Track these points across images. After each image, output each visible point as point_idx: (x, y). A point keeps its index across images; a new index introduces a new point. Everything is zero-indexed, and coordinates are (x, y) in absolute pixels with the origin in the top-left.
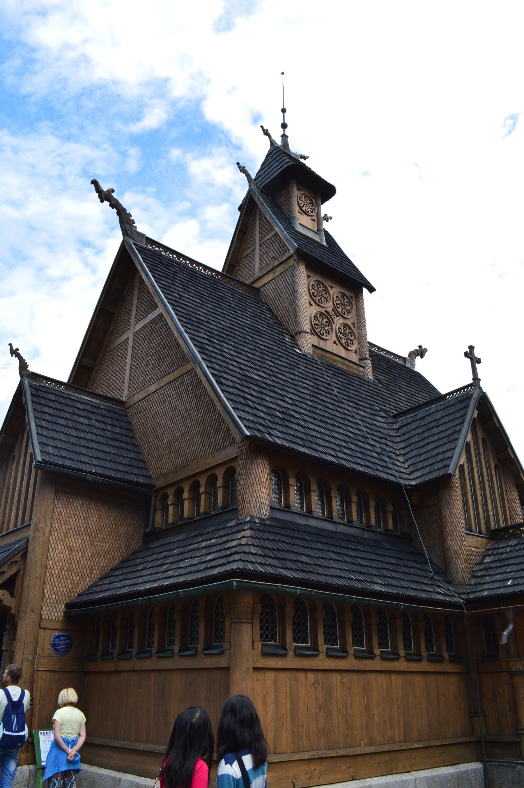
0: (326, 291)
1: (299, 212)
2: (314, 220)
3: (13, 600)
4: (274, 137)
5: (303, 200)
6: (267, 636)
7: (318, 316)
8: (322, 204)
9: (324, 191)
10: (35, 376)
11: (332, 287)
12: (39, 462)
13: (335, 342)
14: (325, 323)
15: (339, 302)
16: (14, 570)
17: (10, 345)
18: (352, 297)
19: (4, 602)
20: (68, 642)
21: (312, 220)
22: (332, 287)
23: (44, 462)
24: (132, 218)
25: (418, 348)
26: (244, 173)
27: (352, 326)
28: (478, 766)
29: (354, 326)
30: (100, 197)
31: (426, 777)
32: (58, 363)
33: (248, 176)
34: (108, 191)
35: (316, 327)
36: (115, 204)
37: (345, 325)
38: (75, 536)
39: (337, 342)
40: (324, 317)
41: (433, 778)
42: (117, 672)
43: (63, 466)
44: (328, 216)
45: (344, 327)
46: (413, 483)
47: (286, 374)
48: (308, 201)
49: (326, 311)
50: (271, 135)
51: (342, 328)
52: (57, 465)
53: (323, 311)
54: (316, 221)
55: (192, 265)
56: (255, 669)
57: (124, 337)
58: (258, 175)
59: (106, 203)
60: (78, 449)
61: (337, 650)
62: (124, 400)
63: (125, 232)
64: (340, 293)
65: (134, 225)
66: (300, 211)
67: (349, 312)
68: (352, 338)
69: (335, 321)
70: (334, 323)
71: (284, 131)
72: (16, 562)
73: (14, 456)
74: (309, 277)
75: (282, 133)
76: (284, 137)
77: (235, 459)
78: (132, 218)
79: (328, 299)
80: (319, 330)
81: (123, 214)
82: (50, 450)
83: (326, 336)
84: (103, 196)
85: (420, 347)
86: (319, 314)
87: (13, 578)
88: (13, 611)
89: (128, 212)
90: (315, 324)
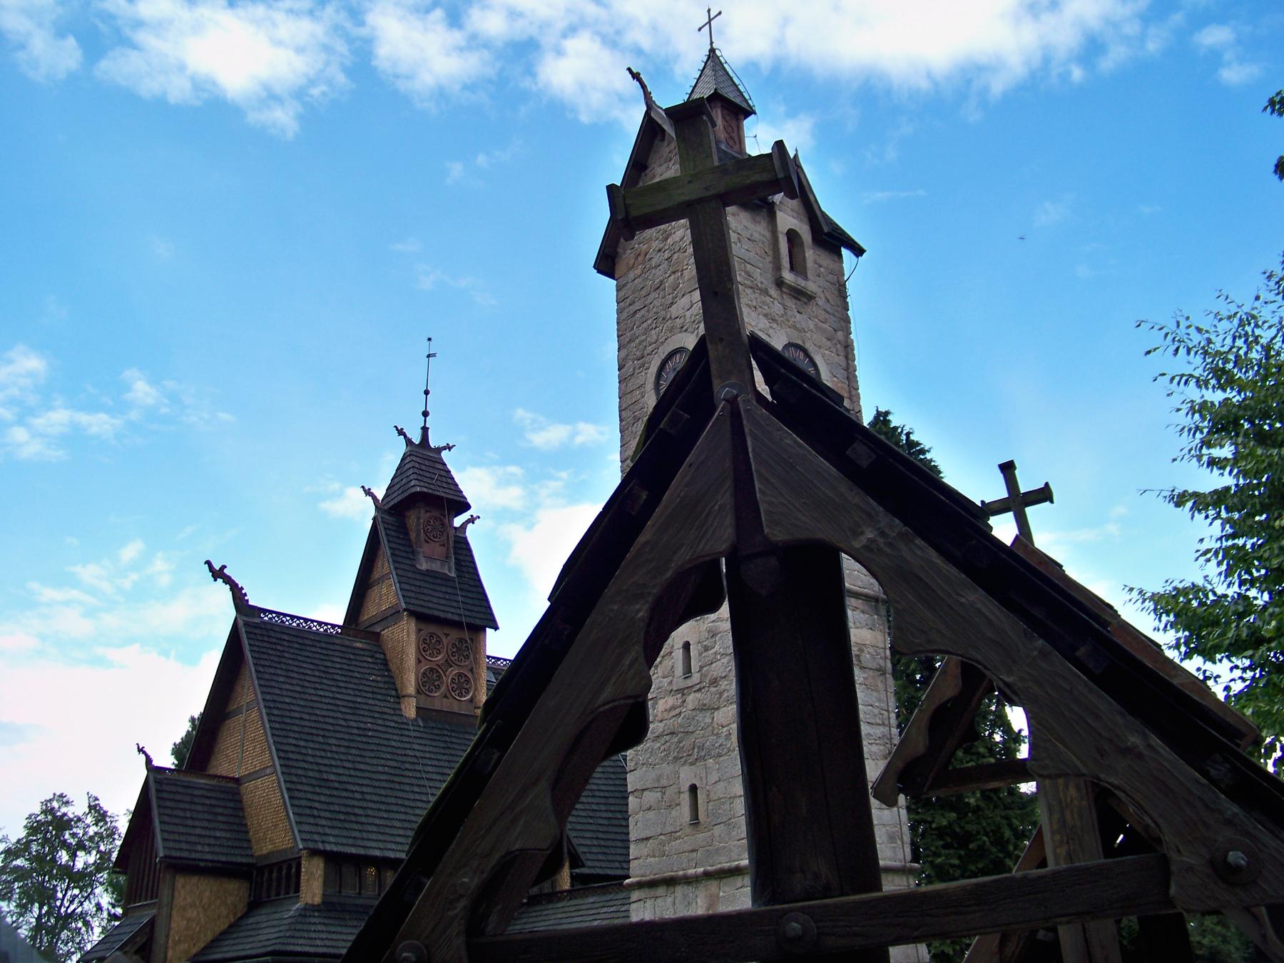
11: (447, 635)
13: (446, 696)
17: (208, 563)
22: (447, 635)
23: (165, 857)
27: (469, 675)
33: (374, 498)
36: (228, 580)
43: (181, 858)
52: (176, 858)
74: (420, 630)
76: (425, 430)
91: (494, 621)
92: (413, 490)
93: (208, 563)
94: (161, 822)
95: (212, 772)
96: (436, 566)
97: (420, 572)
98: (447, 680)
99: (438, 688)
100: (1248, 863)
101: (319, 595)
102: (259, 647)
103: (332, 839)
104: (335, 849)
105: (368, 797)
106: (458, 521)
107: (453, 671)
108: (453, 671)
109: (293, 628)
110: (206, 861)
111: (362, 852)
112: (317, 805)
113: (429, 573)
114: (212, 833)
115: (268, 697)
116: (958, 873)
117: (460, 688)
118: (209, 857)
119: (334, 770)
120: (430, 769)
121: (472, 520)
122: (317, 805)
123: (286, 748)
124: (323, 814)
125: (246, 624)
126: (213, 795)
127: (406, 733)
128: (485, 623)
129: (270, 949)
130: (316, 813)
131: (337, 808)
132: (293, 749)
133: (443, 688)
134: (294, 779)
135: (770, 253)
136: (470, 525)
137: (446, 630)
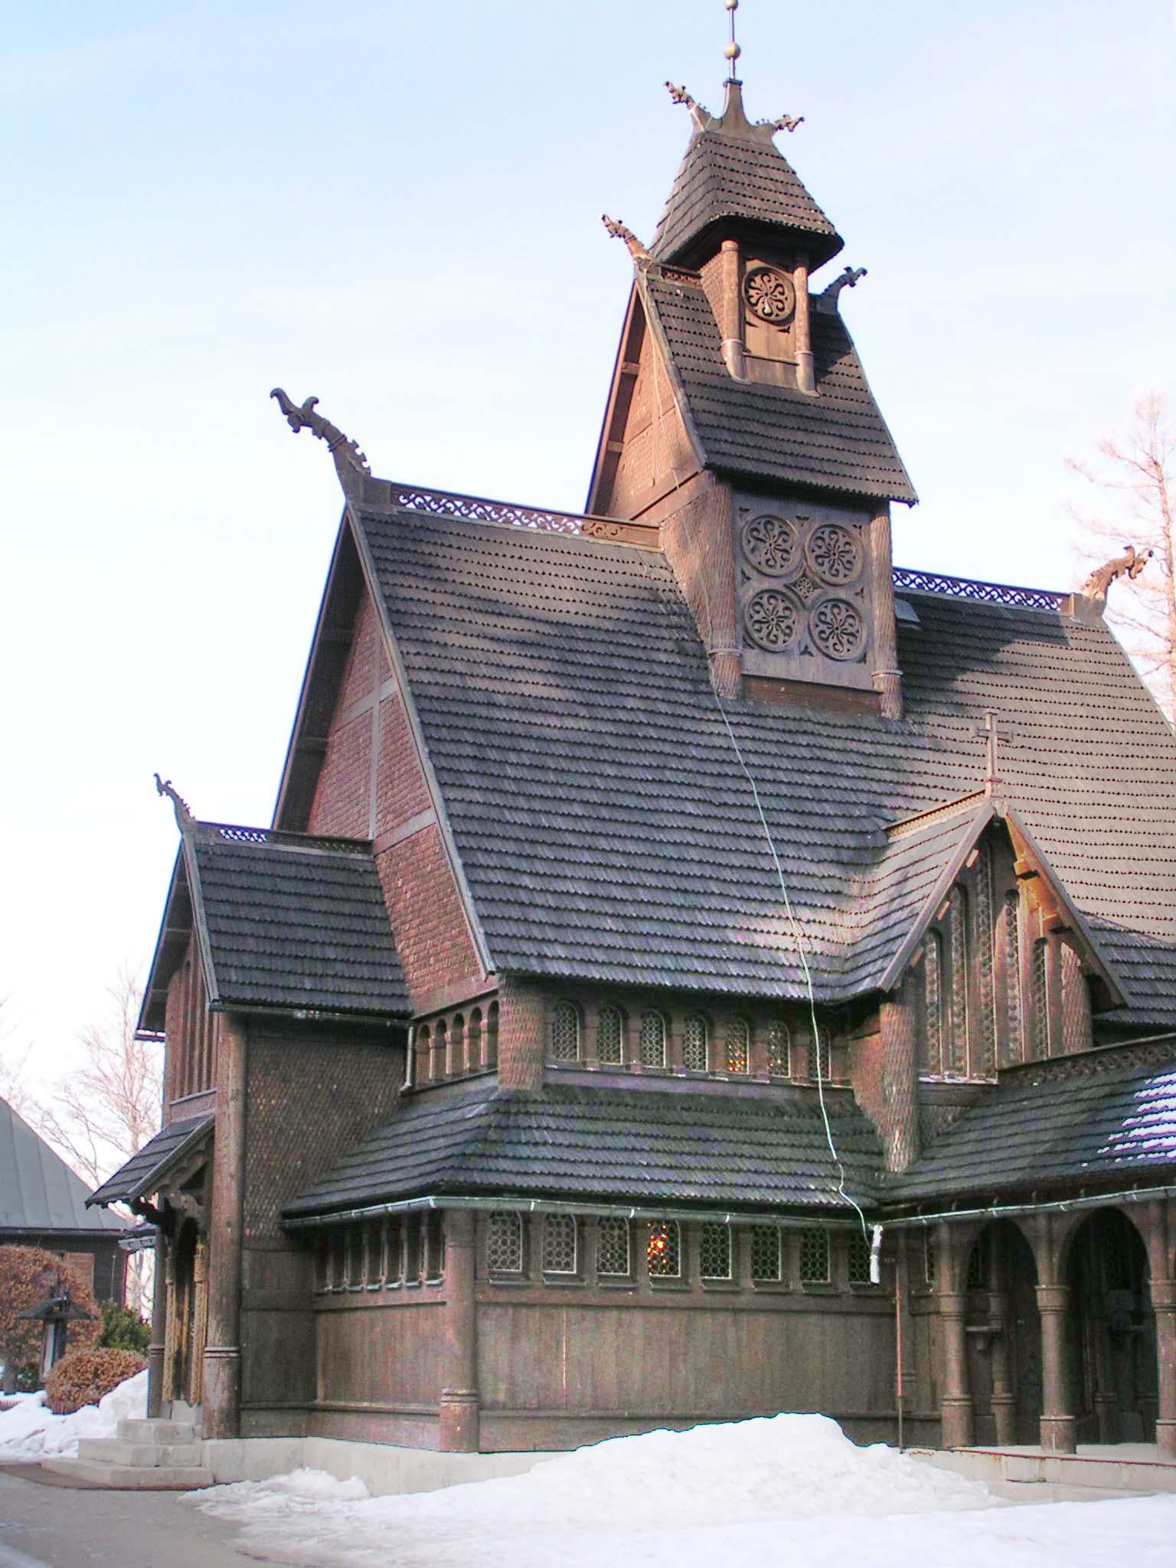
7: (764, 601)
8: (346, 508)
10: (205, 827)
13: (806, 651)
16: (199, 1163)
17: (278, 394)
20: (413, 1315)
24: (358, 452)
27: (856, 602)
30: (290, 422)
32: (246, 795)
35: (757, 626)
36: (324, 430)
38: (850, 841)
39: (812, 649)
42: (344, 1411)
44: (854, 270)
53: (776, 584)
57: (361, 708)
58: (117, 1180)
59: (306, 431)
60: (279, 964)
61: (573, 1276)
62: (370, 838)
65: (365, 465)
72: (199, 1152)
73: (188, 963)
75: (728, 75)
76: (734, 84)
77: (495, 992)
78: (358, 452)
80: (765, 632)
85: (848, 269)
86: (766, 596)
87: (202, 1170)
89: (350, 440)
91: (906, 484)
93: (278, 394)
94: (211, 931)
101: (520, 412)
102: (395, 553)
103: (560, 951)
105: (639, 863)
106: (820, 280)
109: (473, 525)
112: (527, 881)
114: (318, 952)
116: (719, 1247)
119: (565, 809)
121: (849, 278)
122: (527, 881)
124: (539, 899)
125: (364, 519)
129: (430, 1180)
130: (524, 896)
135: (771, 507)
136: (846, 290)
137: (802, 510)
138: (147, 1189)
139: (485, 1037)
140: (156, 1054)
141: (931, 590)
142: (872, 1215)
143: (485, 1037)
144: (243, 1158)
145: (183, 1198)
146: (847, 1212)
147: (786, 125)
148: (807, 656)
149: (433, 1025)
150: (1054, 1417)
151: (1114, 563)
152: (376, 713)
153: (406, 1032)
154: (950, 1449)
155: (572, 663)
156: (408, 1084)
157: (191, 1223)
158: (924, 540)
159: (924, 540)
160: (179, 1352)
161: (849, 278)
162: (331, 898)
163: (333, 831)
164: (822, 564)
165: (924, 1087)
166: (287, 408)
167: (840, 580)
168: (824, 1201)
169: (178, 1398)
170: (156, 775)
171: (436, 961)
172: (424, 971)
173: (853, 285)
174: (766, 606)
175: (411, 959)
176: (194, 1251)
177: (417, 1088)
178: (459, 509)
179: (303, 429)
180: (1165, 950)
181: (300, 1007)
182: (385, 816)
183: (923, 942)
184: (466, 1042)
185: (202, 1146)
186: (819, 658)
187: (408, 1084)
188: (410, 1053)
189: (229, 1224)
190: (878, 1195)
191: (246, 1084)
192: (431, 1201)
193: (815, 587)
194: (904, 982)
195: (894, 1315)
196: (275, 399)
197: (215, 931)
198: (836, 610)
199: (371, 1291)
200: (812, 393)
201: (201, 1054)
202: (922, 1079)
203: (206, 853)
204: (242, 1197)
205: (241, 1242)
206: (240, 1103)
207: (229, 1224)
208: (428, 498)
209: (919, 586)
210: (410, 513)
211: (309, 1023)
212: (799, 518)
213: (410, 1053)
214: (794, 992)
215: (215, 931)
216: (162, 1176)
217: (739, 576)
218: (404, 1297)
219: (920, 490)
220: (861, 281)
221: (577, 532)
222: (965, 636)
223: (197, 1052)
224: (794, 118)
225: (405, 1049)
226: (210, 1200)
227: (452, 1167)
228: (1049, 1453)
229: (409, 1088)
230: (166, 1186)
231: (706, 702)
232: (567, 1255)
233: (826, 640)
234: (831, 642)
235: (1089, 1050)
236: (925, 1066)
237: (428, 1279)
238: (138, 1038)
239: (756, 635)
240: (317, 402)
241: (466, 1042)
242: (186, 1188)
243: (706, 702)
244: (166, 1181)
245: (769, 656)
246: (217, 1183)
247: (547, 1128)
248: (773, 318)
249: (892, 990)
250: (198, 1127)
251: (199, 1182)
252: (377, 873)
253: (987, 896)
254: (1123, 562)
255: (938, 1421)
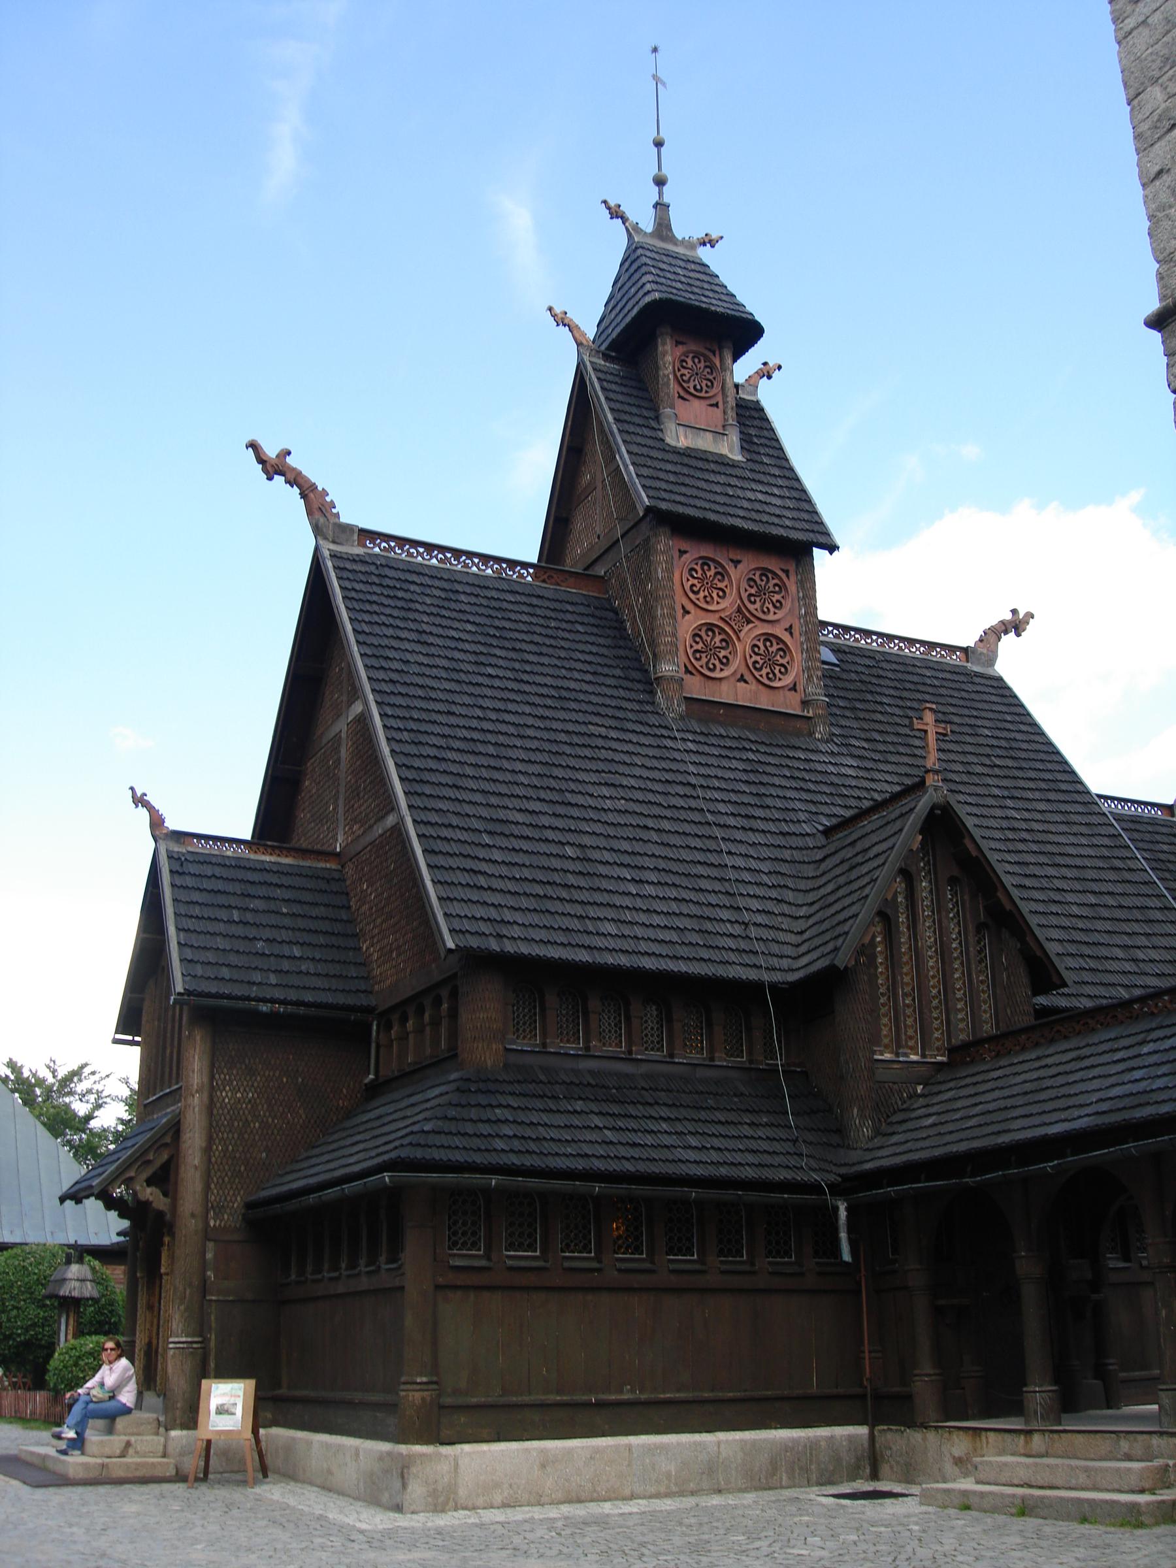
0: (722, 574)
1: (680, 397)
2: (716, 405)
3: (168, 1201)
4: (632, 217)
5: (690, 363)
6: (568, 1246)
7: (703, 634)
8: (735, 361)
9: (743, 332)
10: (180, 836)
11: (736, 563)
12: (179, 994)
13: (742, 679)
14: (718, 644)
15: (753, 591)
17: (253, 446)
18: (787, 572)
19: (154, 1205)
21: (712, 405)
22: (736, 563)
23: (188, 992)
24: (328, 499)
25: (1008, 616)
26: (565, 325)
27: (786, 637)
28: (863, 1430)
29: (791, 634)
30: (265, 471)
31: (741, 1440)
34: (277, 456)
35: (698, 655)
36: (296, 479)
37: (768, 637)
39: (748, 677)
40: (717, 631)
41: (754, 1443)
45: (766, 640)
46: (792, 977)
47: (590, 789)
48: (702, 365)
49: (721, 618)
50: (628, 214)
51: (761, 644)
52: (209, 995)
53: (713, 619)
54: (720, 404)
55: (457, 558)
56: (438, 1287)
59: (279, 480)
63: (317, 530)
64: (757, 569)
65: (334, 511)
66: (682, 393)
67: (778, 605)
68: (784, 661)
69: (742, 635)
70: (739, 639)
71: (660, 194)
72: (166, 1145)
75: (655, 198)
76: (661, 207)
77: (455, 975)
78: (328, 499)
79: (727, 591)
80: (704, 660)
81: (311, 495)
82: (199, 970)
83: (722, 670)
84: (270, 469)
85: (1014, 612)
86: (704, 629)
88: (168, 1217)
89: (320, 488)
90: (696, 651)
91: (827, 534)
92: (647, 299)
93: (253, 446)
94: (178, 929)
95: (294, 843)
96: (705, 443)
97: (676, 451)
98: (743, 646)
99: (725, 662)
100: (77, 1433)
101: (482, 488)
102: (363, 616)
104: (525, 949)
106: (743, 369)
107: (750, 634)
108: (750, 634)
110: (273, 1001)
111: (584, 956)
113: (688, 453)
115: (381, 675)
117: (771, 662)
118: (278, 994)
120: (722, 808)
121: (766, 372)
123: (417, 763)
124: (497, 884)
126: (286, 881)
127: (669, 743)
128: (811, 537)
130: (482, 881)
131: (527, 873)
132: (432, 764)
133: (736, 664)
134: (434, 818)
136: (1008, 641)
138: (113, 1180)
139: (445, 1023)
140: (133, 1055)
141: (849, 640)
142: (837, 1190)
143: (445, 1023)
144: (208, 1150)
145: (149, 1190)
146: (815, 1188)
147: (709, 241)
148: (743, 684)
149: (395, 1017)
150: (1039, 1393)
151: (1002, 622)
152: (343, 735)
153: (371, 1025)
154: (925, 1426)
155: (528, 682)
156: (371, 1077)
157: (160, 1214)
158: (851, 590)
159: (851, 590)
160: (149, 1344)
161: (766, 372)
162: (300, 902)
163: (304, 845)
164: (755, 602)
165: (879, 1065)
166: (261, 460)
167: (771, 617)
168: (789, 1177)
169: (149, 1389)
170: (132, 789)
171: (398, 955)
172: (387, 966)
173: (769, 377)
174: (705, 637)
175: (375, 956)
176: (162, 1244)
177: (381, 1080)
178: (421, 555)
179: (276, 477)
180: (349, 1496)
181: (264, 1000)
182: (351, 828)
183: (872, 923)
184: (428, 1029)
185: (168, 1140)
186: (754, 686)
187: (371, 1077)
188: (373, 1046)
189: (193, 1215)
190: (843, 1170)
191: (212, 1078)
192: (387, 1177)
193: (749, 622)
194: (857, 961)
195: (860, 1291)
196: (250, 449)
197: (183, 930)
198: (768, 644)
199: (331, 1279)
200: (739, 458)
201: (172, 1053)
202: (876, 1057)
203: (179, 859)
204: (207, 1188)
205: (207, 1234)
206: (205, 1095)
207: (193, 1215)
208: (393, 544)
209: (836, 636)
210: (377, 555)
211: (273, 1015)
212: (732, 561)
213: (373, 1046)
214: (752, 975)
215: (183, 930)
216: (126, 1169)
217: (680, 612)
218: (364, 1283)
219: (838, 538)
220: (776, 375)
221: (529, 578)
222: (879, 677)
223: (168, 1051)
224: (714, 236)
225: (369, 1044)
226: (176, 1191)
227: (411, 1144)
228: (1034, 1426)
229: (373, 1080)
230: (131, 1179)
231: (653, 720)
232: (530, 1236)
233: (760, 669)
234: (702, 594)
235: (1033, 1022)
236: (878, 1044)
237: (387, 1263)
238: (116, 1041)
239: (751, 607)
240: (289, 453)
241: (428, 1029)
242: (149, 1182)
243: (653, 720)
244: (132, 1174)
245: (710, 682)
246: (182, 1174)
247: (508, 1106)
248: (703, 394)
249: (846, 967)
250: (164, 1120)
251: (165, 1178)
252: (344, 880)
253: (930, 882)
254: (1010, 622)
255: (909, 1397)
